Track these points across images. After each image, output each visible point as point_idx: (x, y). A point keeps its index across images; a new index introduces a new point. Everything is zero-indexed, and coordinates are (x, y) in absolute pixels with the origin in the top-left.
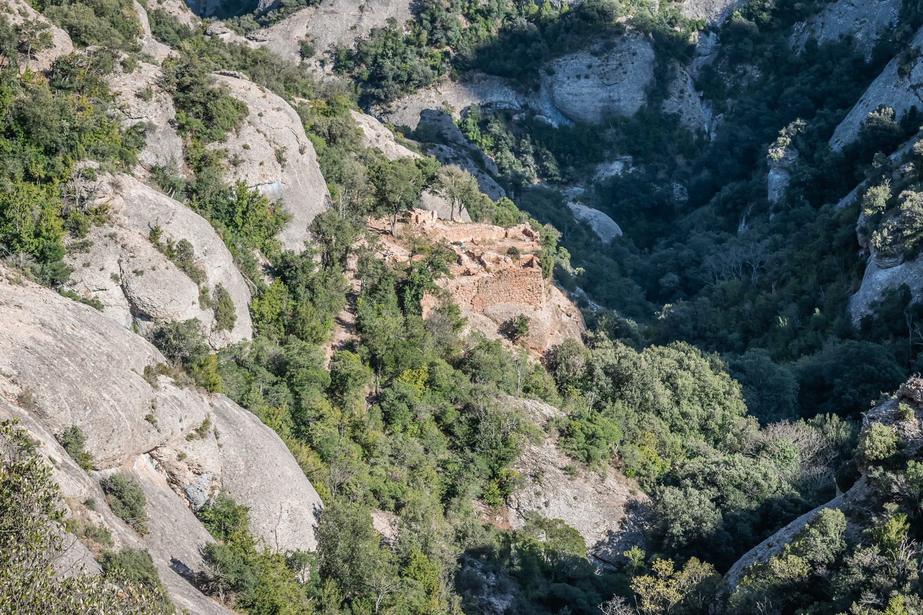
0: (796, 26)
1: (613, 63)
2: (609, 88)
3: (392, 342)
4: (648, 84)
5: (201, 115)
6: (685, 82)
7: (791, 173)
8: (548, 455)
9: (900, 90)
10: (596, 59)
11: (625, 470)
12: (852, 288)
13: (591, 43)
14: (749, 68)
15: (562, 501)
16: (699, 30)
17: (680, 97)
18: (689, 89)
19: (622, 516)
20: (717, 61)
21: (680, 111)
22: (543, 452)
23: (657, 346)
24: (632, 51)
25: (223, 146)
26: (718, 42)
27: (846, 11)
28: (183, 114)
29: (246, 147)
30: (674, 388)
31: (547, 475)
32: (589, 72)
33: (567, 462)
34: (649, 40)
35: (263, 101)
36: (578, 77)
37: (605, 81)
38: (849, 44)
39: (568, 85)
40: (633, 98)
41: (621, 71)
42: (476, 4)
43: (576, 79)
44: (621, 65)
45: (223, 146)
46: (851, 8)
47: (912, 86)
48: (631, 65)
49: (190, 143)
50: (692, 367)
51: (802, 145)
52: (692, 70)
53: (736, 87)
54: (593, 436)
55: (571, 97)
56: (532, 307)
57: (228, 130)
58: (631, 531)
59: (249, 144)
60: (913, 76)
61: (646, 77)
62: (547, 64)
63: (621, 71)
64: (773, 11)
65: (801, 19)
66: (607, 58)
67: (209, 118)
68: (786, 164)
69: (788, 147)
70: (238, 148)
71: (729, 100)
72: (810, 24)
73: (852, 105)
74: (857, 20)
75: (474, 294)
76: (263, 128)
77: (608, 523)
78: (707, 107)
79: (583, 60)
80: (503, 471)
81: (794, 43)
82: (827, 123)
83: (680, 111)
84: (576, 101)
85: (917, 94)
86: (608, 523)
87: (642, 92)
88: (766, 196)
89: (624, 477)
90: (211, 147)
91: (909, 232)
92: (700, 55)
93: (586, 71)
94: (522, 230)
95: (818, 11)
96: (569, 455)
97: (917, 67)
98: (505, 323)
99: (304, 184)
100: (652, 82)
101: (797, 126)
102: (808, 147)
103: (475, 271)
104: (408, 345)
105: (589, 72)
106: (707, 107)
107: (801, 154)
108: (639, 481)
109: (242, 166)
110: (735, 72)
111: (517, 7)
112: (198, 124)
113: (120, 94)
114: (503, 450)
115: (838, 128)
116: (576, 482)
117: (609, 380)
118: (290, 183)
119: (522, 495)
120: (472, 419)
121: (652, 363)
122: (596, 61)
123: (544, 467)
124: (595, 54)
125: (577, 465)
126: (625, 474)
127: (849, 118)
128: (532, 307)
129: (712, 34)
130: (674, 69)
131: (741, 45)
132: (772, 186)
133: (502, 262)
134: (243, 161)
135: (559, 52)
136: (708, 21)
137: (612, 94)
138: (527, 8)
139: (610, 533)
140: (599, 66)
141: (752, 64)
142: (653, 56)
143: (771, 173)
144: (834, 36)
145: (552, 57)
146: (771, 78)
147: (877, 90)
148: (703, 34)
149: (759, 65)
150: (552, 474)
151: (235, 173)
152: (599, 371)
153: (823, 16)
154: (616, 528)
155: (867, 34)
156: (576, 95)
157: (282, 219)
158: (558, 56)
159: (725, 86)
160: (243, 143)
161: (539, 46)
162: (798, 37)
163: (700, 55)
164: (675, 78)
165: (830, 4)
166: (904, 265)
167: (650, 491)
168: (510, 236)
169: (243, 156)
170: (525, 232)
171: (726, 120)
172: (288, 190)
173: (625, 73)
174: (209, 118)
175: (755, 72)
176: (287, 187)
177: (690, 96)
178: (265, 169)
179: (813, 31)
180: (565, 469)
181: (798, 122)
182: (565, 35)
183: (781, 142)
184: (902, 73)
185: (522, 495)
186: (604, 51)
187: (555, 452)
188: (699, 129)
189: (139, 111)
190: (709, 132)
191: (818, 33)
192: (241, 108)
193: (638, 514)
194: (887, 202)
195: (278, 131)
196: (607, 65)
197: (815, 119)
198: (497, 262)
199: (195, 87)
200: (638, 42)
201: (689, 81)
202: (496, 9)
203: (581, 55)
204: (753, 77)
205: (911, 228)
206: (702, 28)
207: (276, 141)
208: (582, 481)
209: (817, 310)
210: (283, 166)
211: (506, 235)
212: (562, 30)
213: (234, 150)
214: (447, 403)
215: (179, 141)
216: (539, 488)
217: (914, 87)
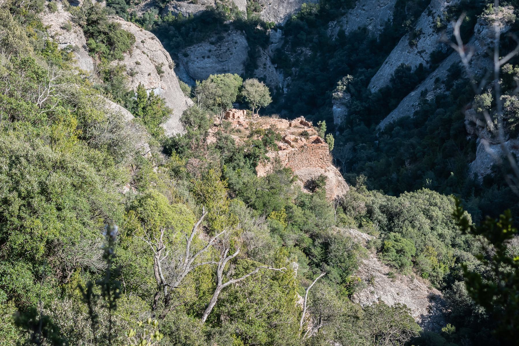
0: (331, 24)
1: (224, 49)
2: (222, 63)
3: (260, 193)
4: (245, 60)
5: (105, 41)
6: (266, 59)
7: (347, 107)
8: (375, 265)
9: (411, 55)
10: (213, 46)
11: (421, 272)
12: (469, 159)
13: (209, 37)
14: (304, 49)
15: (389, 297)
16: (271, 28)
17: (265, 68)
18: (269, 63)
19: (428, 305)
20: (284, 45)
21: (265, 76)
22: (371, 264)
23: (409, 192)
24: (234, 41)
25: (122, 63)
26: (283, 35)
27: (360, 14)
28: (91, 41)
29: (137, 63)
30: (431, 218)
31: (377, 279)
32: (210, 54)
33: (387, 269)
34: (244, 35)
35: (141, 33)
36: (203, 57)
37: (220, 60)
38: (365, 32)
39: (198, 62)
40: (237, 69)
41: (230, 53)
42: (135, 16)
43: (202, 59)
44: (228, 49)
45: (122, 63)
46: (364, 12)
47: (418, 52)
48: (234, 49)
49: (98, 62)
50: (439, 204)
51: (353, 90)
52: (269, 52)
53: (297, 61)
54: (401, 251)
55: (199, 70)
56: (323, 170)
57: (124, 52)
58: (435, 315)
59: (139, 61)
60: (419, 46)
61: (244, 57)
62: (183, 51)
63: (230, 53)
64: (316, 15)
65: (333, 20)
66: (220, 46)
67: (111, 43)
68: (344, 101)
69: (344, 91)
70: (133, 65)
71: (293, 69)
72: (339, 22)
73: (381, 64)
74: (368, 18)
75: (286, 163)
76: (146, 51)
77: (420, 310)
78: (280, 73)
79: (205, 47)
80: (350, 278)
81: (330, 34)
82: (365, 77)
83: (265, 76)
84: (203, 72)
85: (422, 57)
86: (420, 310)
87: (242, 66)
88: (333, 121)
89: (421, 278)
90: (114, 64)
91: (512, 120)
92: (272, 43)
93: (208, 54)
94: (299, 121)
95: (343, 14)
96: (387, 265)
97: (420, 41)
98: (308, 181)
99: (174, 89)
100: (247, 60)
101: (348, 79)
102: (357, 91)
103: (285, 147)
104: (271, 194)
105: (210, 54)
106: (280, 73)
107: (352, 96)
108: (431, 280)
109: (136, 76)
110: (295, 52)
111: (161, 18)
112: (103, 48)
113: (50, 27)
114: (348, 262)
115: (373, 79)
116: (396, 283)
117: (385, 216)
118: (166, 89)
119: (362, 294)
120: (323, 244)
121: (406, 201)
122: (213, 48)
123: (374, 274)
124: (212, 43)
125: (394, 271)
126: (421, 276)
127: (379, 73)
128: (323, 170)
129: (278, 30)
130: (259, 51)
131: (299, 36)
132: (336, 115)
133: (299, 141)
134: (137, 73)
135: (191, 43)
136: (276, 23)
137: (224, 67)
138: (167, 18)
139: (422, 316)
140: (216, 50)
141: (306, 47)
142: (247, 44)
143: (335, 107)
144: (355, 28)
145: (186, 46)
146: (318, 54)
147: (397, 55)
148: (273, 31)
149: (310, 47)
150: (380, 278)
151: (132, 81)
152: (377, 211)
153: (347, 17)
154: (425, 313)
155: (375, 26)
156: (203, 68)
157: (167, 113)
158: (190, 46)
159: (291, 60)
160: (135, 60)
161: (178, 39)
162: (333, 30)
163: (272, 43)
164: (260, 56)
165: (350, 10)
166: (509, 141)
167: (439, 287)
168: (292, 125)
169: (137, 70)
170: (301, 123)
171: (293, 80)
172: (166, 93)
173: (231, 54)
174: (111, 43)
175: (308, 51)
176: (165, 92)
177: (270, 67)
178: (152, 78)
179: (342, 26)
180: (388, 274)
181: (348, 76)
182: (193, 33)
183: (340, 88)
184: (411, 45)
185: (362, 294)
186: (218, 42)
187: (378, 263)
188: (277, 86)
189: (65, 38)
190: (283, 88)
191: (345, 27)
192: (131, 36)
193: (436, 302)
194: (492, 103)
195: (156, 53)
196: (220, 50)
197: (357, 75)
198: (296, 140)
199: (101, 22)
200: (238, 35)
201: (268, 58)
202: (148, 19)
203: (203, 44)
204: (307, 54)
205: (514, 117)
206: (273, 27)
207: (155, 60)
208: (399, 282)
209: (452, 173)
210: (161, 77)
211: (290, 125)
212: (191, 30)
213: (130, 65)
214: (302, 233)
215: (90, 60)
216: (372, 289)
217: (420, 53)
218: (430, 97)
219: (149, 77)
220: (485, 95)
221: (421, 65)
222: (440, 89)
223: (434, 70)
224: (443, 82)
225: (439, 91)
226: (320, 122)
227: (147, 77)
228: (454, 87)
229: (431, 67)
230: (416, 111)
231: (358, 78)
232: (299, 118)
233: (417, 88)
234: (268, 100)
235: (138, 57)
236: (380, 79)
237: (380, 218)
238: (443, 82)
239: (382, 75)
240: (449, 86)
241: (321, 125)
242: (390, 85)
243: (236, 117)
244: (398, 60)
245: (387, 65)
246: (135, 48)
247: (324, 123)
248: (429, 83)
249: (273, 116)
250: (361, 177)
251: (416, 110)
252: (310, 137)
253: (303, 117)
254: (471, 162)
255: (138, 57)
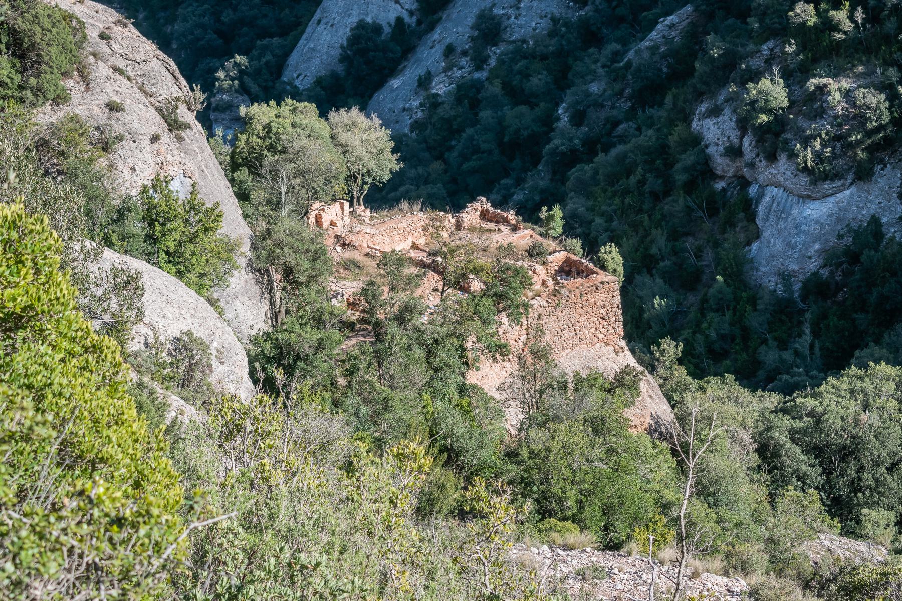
29: (113, 107)
57: (65, 74)
70: (102, 116)
82: (274, 56)
101: (236, 64)
134: (119, 138)
160: (104, 99)
218: (441, 88)
219: (156, 146)
220: (765, 83)
221: (399, 20)
222: (461, 68)
223: (432, 27)
224: (464, 53)
225: (458, 73)
226: (545, 209)
227: (148, 148)
228: (493, 62)
229: (419, 22)
230: (416, 122)
231: (259, 59)
232: (476, 205)
233: (402, 70)
234: (388, 165)
235: (109, 88)
236: (309, 59)
237: (804, 468)
238: (464, 53)
239: (313, 49)
240: (479, 62)
241: (550, 218)
242: (340, 69)
243: (325, 226)
244: (347, 13)
245: (322, 26)
246: (91, 59)
247: (557, 212)
248: (429, 56)
249: (405, 205)
250: (664, 346)
251: (415, 117)
252: (550, 258)
253: (484, 199)
254: (749, 244)
255: (109, 88)
